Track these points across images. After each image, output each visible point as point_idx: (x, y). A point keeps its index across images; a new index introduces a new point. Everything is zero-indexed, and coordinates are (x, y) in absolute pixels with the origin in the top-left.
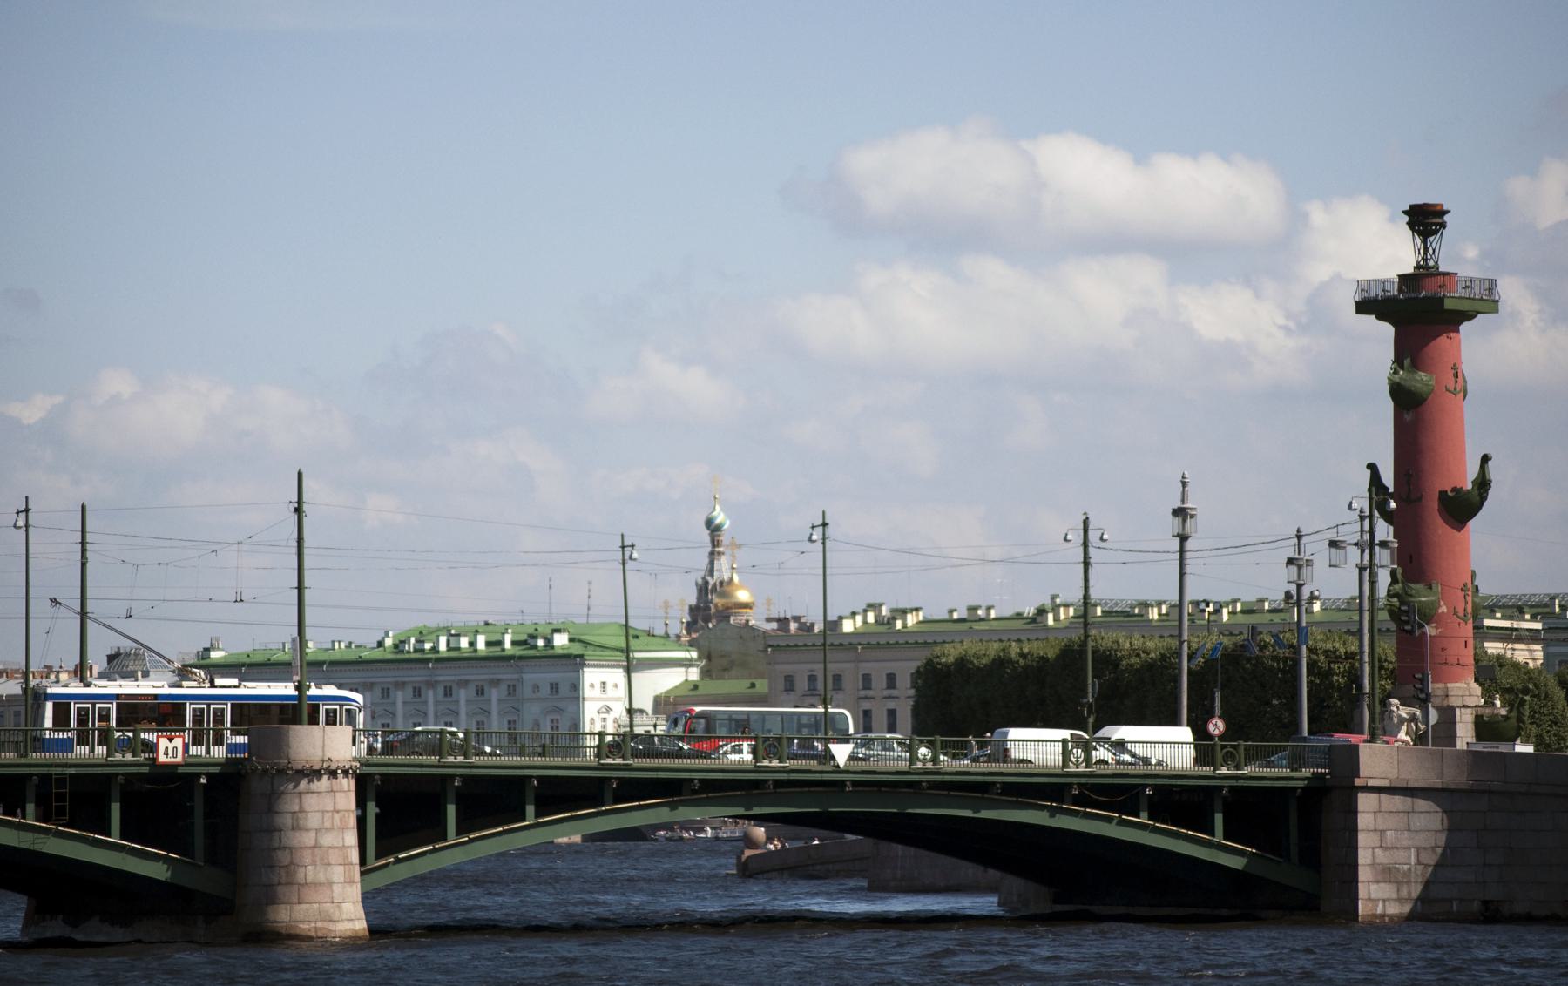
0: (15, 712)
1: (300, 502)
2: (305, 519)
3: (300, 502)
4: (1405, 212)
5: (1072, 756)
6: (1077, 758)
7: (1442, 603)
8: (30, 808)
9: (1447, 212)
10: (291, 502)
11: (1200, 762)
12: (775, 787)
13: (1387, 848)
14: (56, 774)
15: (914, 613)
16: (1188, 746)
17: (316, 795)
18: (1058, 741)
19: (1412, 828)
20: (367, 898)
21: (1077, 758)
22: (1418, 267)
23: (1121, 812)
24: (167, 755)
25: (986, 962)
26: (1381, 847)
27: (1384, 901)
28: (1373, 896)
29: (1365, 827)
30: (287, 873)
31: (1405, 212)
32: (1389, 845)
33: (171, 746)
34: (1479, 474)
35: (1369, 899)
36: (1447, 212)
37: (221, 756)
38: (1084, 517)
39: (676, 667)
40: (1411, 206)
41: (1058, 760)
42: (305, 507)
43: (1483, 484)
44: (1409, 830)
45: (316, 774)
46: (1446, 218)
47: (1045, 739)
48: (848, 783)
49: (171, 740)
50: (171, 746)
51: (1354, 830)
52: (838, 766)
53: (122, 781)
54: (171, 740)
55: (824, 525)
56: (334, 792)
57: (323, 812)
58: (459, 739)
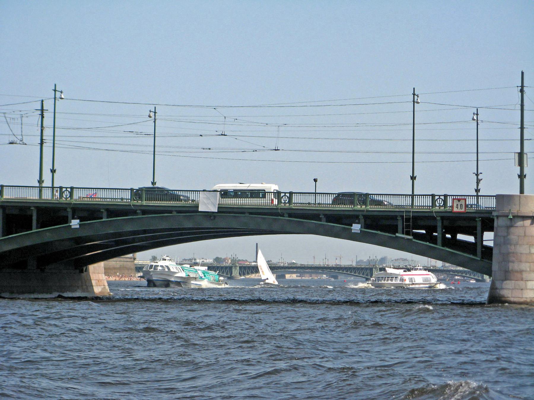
1: (522, 86)
2: (524, 95)
3: (522, 86)
5: (64, 194)
6: (440, 204)
8: (406, 230)
10: (518, 87)
11: (335, 203)
12: (284, 214)
15: (44, 141)
16: (473, 197)
18: (129, 189)
21: (440, 204)
24: (458, 208)
25: (506, 329)
33: (459, 204)
37: (24, 197)
39: (519, 159)
41: (37, 197)
42: (525, 89)
47: (111, 188)
53: (137, 212)
56: (525, 227)
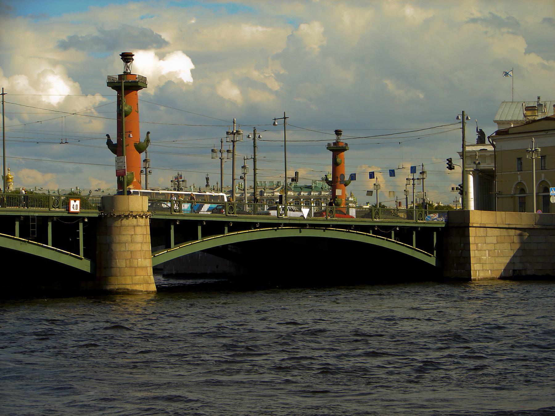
0: (182, 178)
4: (120, 55)
7: (135, 178)
8: (371, 231)
9: (134, 55)
13: (479, 250)
14: (31, 216)
17: (140, 227)
19: (487, 243)
20: (157, 270)
22: (124, 72)
23: (387, 238)
26: (477, 250)
27: (479, 270)
28: (475, 269)
29: (472, 243)
30: (130, 262)
31: (120, 55)
32: (479, 249)
34: (146, 138)
35: (474, 270)
36: (134, 55)
38: (254, 129)
40: (122, 53)
43: (148, 141)
44: (485, 243)
45: (127, 217)
46: (133, 57)
48: (307, 225)
49: (75, 201)
50: (75, 204)
51: (469, 244)
52: (304, 218)
54: (75, 201)
55: (285, 118)
57: (143, 234)
58: (184, 202)
